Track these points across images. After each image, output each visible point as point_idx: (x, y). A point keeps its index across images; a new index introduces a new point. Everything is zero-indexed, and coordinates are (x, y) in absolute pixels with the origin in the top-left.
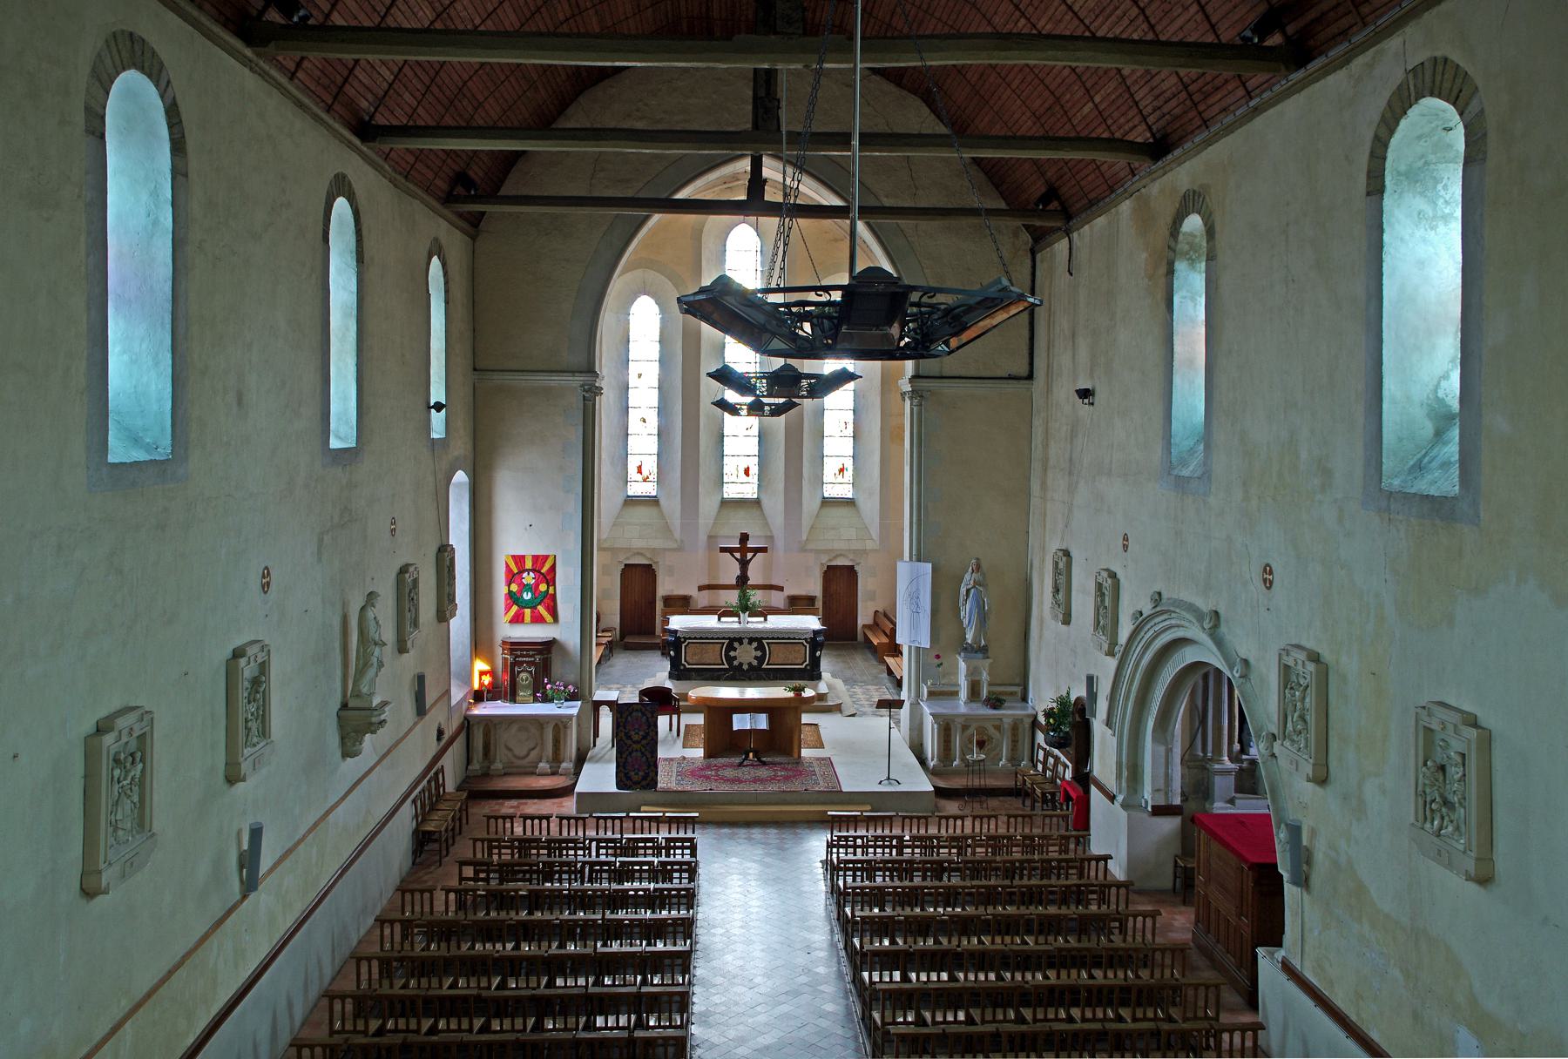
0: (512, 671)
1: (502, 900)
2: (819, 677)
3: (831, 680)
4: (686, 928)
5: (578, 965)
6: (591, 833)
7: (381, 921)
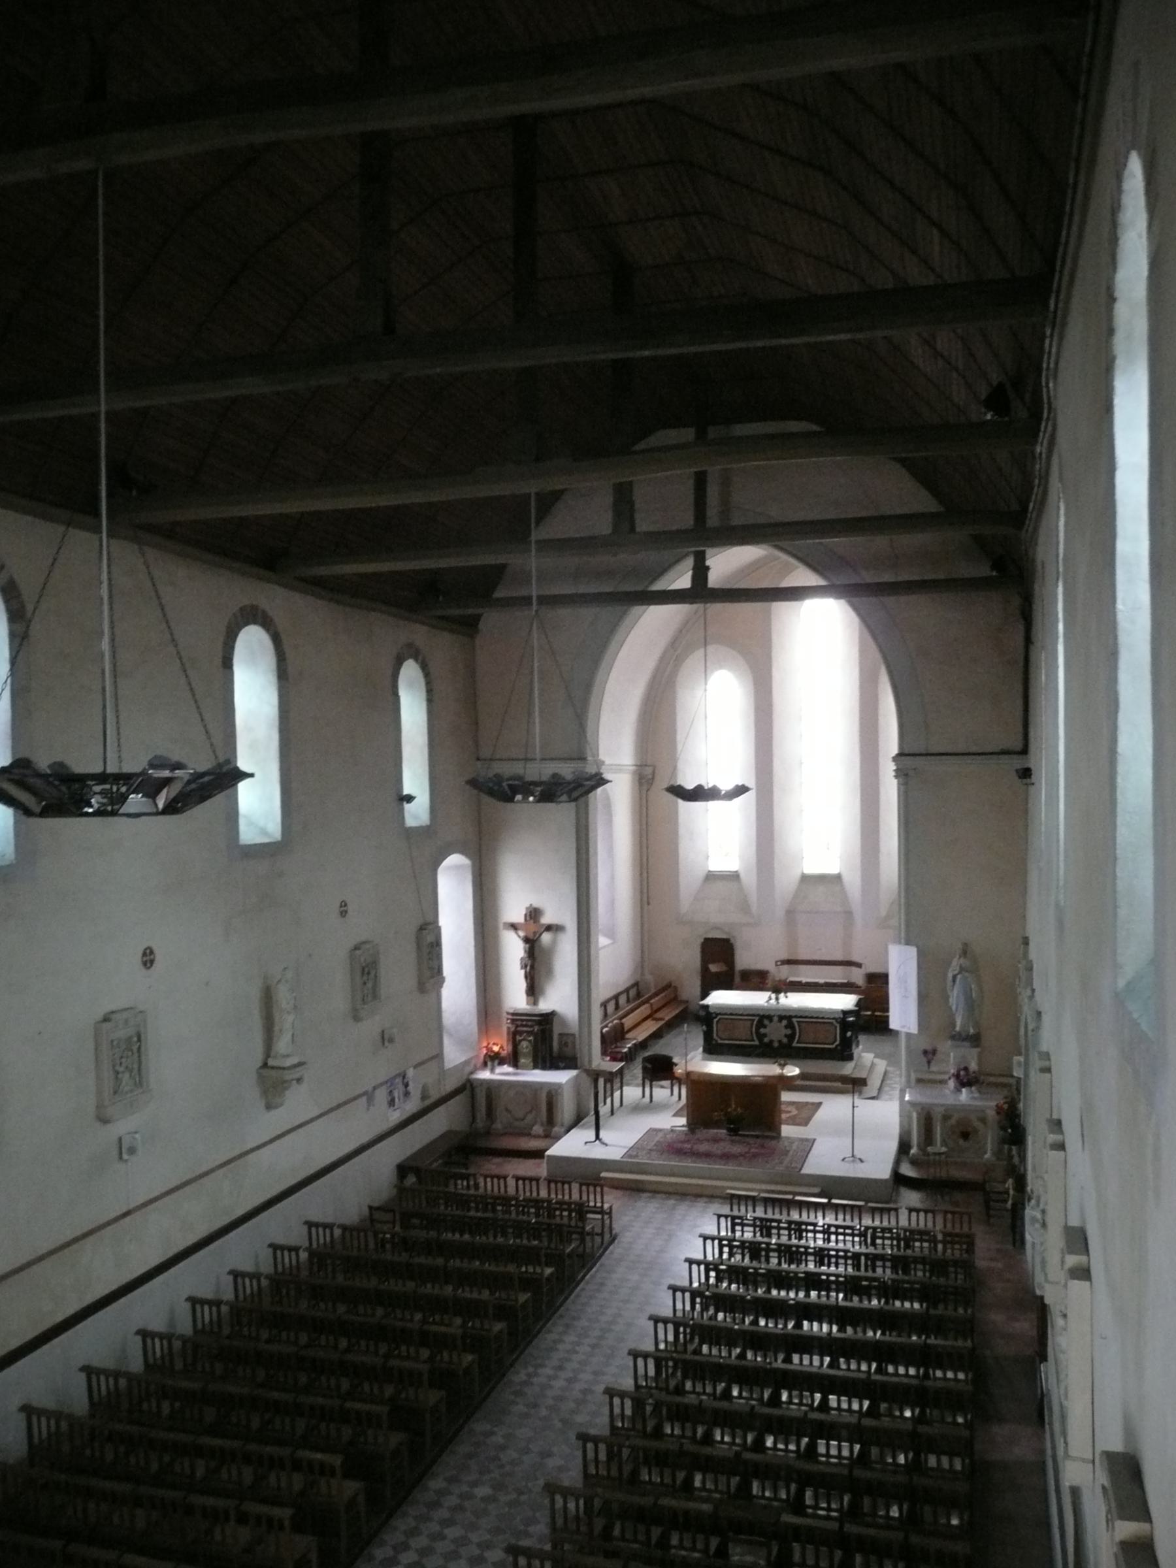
0: (514, 1039)
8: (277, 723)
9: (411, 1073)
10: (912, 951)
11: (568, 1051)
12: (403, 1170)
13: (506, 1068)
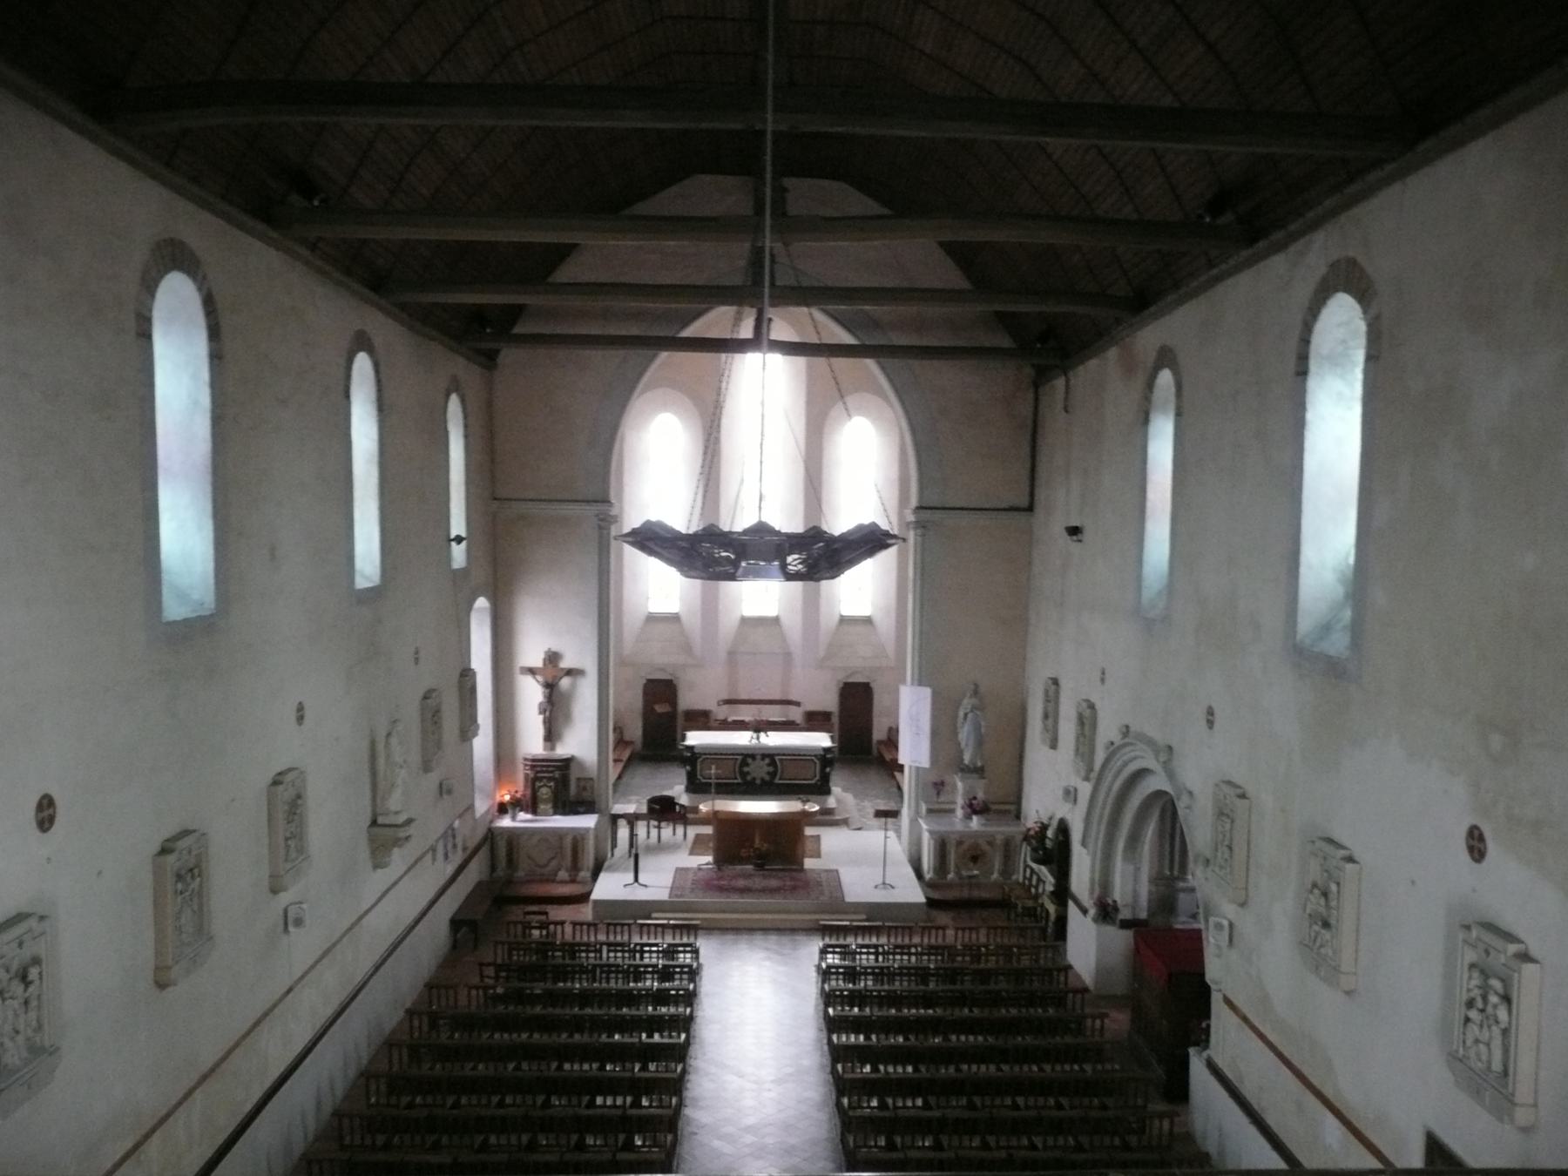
1: (519, 997)
2: (828, 792)
3: (840, 795)
4: (686, 1023)
5: (586, 1053)
6: (602, 937)
7: (410, 1013)
8: (376, 459)
9: (457, 824)
10: (927, 692)
11: (586, 795)
12: (456, 924)
13: (522, 815)
